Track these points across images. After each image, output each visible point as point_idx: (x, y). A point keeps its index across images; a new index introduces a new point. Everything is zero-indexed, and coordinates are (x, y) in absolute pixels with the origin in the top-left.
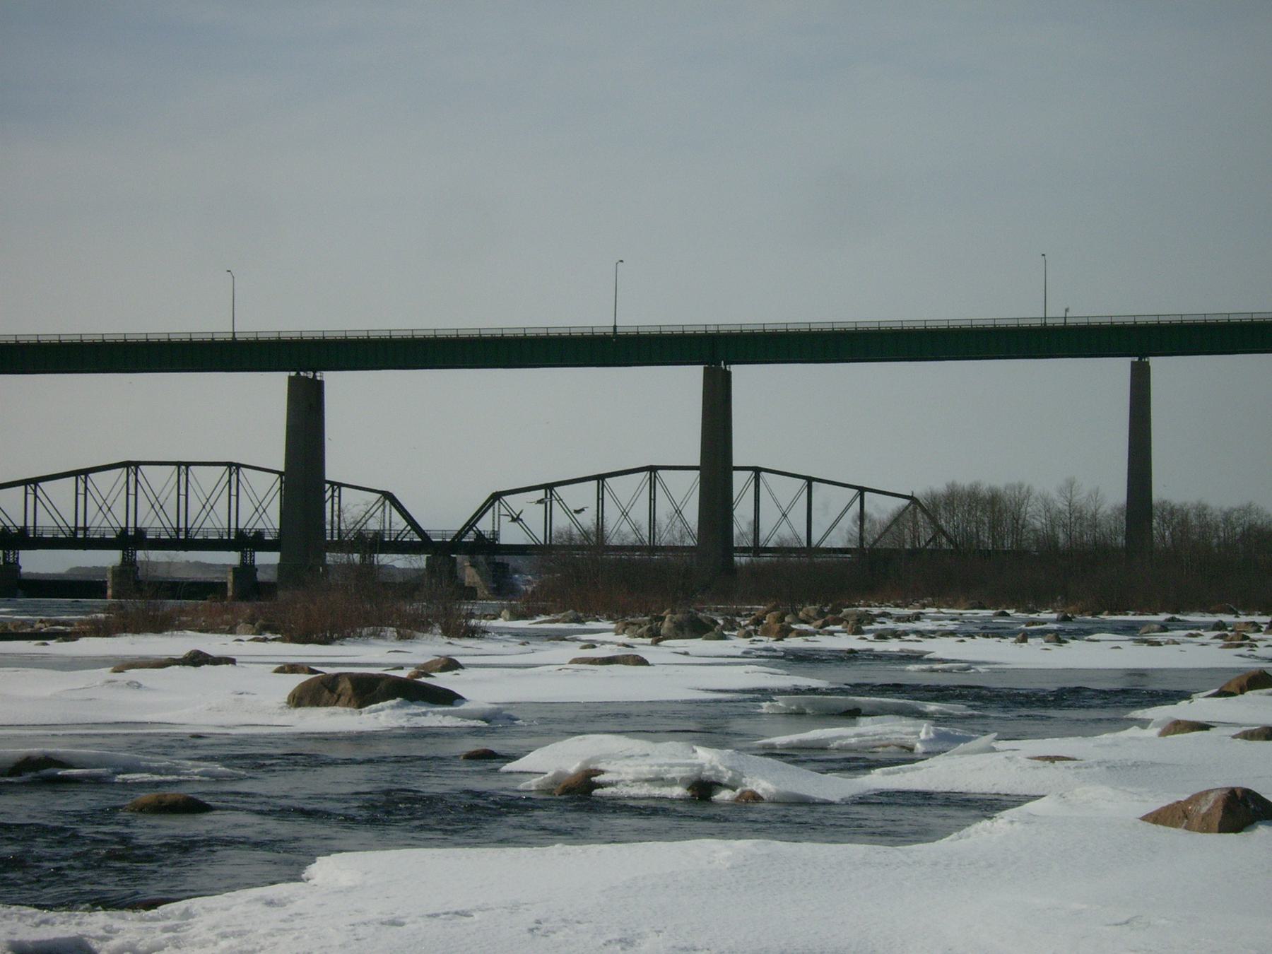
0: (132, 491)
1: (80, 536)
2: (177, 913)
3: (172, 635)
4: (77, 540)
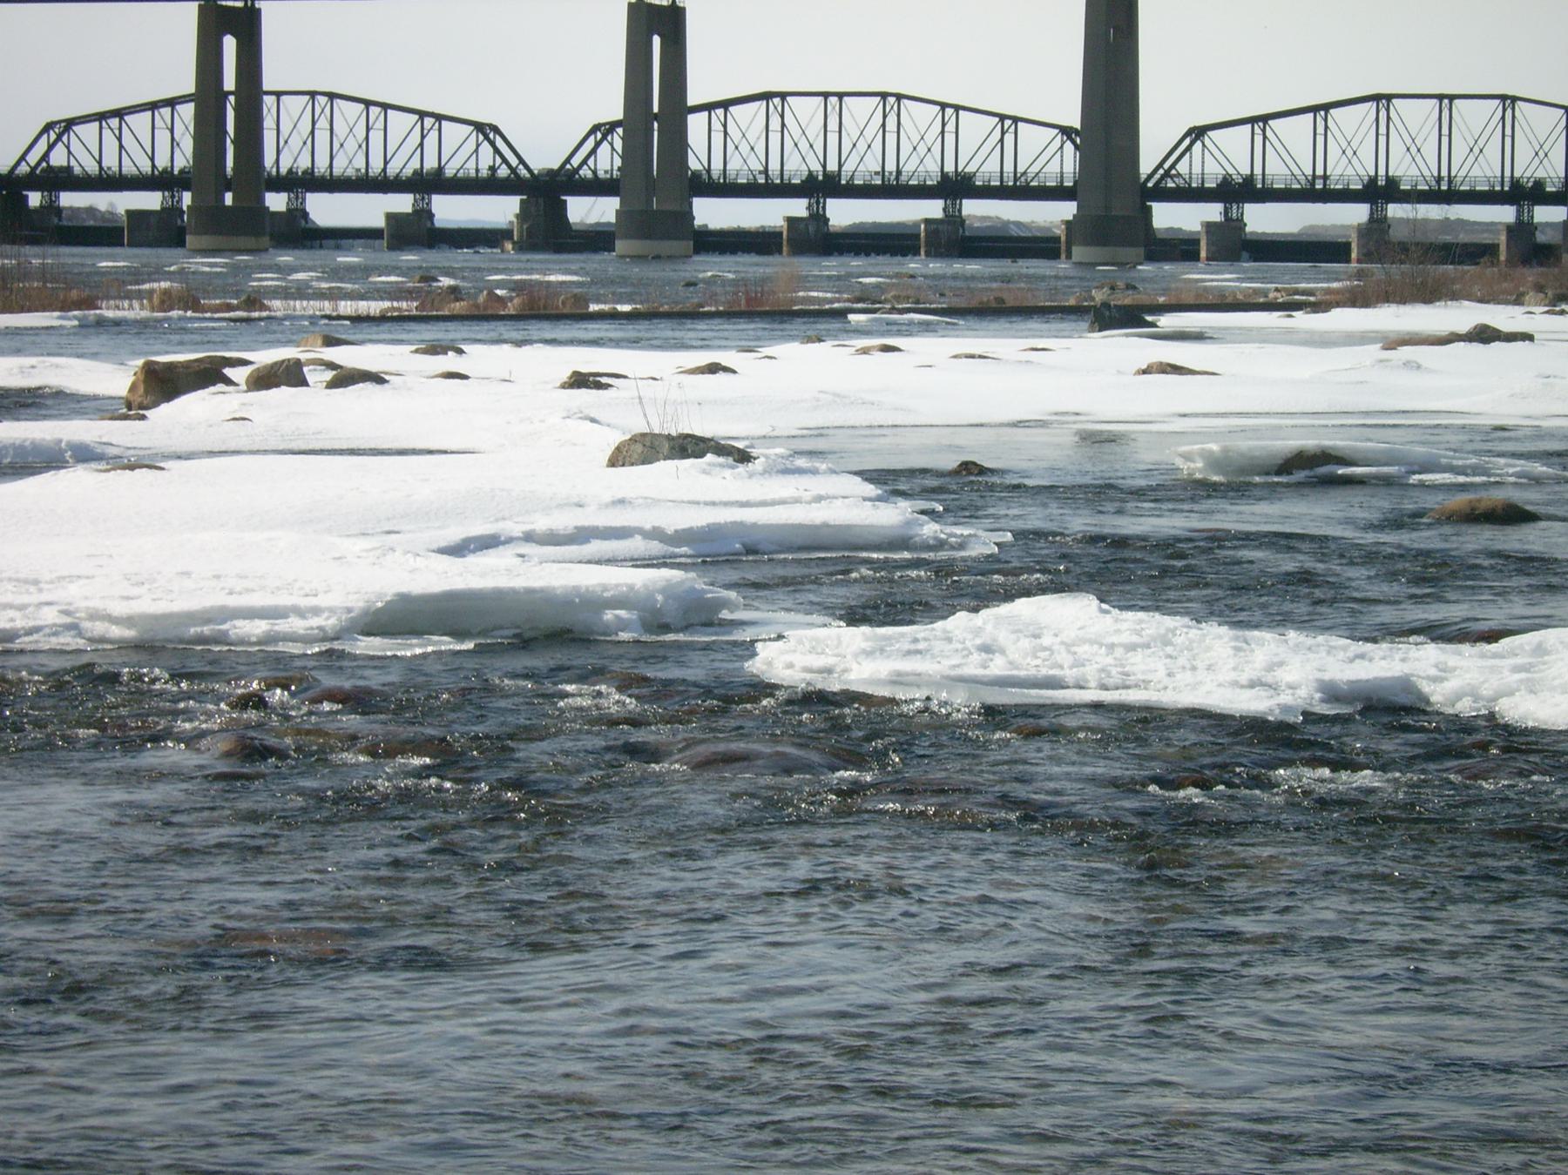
0: (1383, 130)
1: (1319, 186)
2: (1527, 648)
3: (1446, 306)
4: (1315, 192)
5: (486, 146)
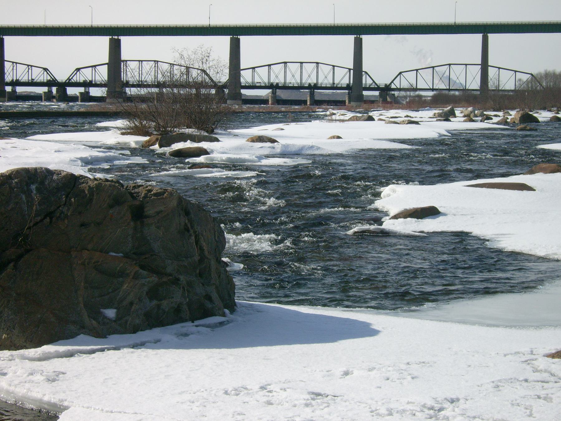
5: (45, 73)
